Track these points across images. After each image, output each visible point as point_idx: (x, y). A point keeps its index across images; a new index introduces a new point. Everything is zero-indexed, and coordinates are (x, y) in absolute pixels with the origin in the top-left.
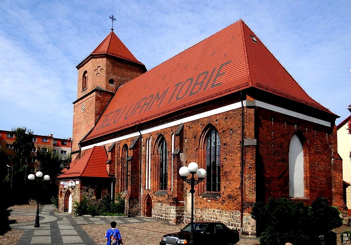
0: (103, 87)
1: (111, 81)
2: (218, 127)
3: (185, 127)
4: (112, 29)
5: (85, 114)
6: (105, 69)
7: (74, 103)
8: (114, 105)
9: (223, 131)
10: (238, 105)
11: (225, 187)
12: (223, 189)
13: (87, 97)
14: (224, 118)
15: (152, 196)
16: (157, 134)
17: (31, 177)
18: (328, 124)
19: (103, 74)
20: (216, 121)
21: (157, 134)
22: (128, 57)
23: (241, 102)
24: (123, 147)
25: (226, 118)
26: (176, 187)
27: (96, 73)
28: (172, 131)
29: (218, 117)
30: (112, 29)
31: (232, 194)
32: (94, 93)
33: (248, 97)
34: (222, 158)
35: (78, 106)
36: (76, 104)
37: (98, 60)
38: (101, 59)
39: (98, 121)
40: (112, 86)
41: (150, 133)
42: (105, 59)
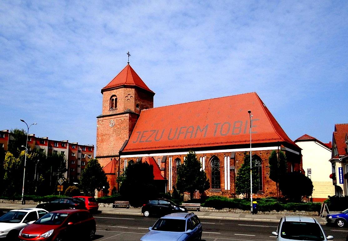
0: (133, 110)
1: (137, 106)
2: (262, 157)
3: (236, 154)
4: (128, 63)
5: (115, 128)
6: (134, 97)
7: (97, 117)
8: (140, 123)
9: (265, 160)
10: (276, 148)
11: (267, 188)
12: (266, 189)
13: (117, 116)
14: (266, 153)
15: (208, 193)
16: (211, 155)
17: (71, 192)
18: (298, 153)
19: (133, 100)
20: (261, 154)
21: (211, 155)
22: (142, 85)
23: (278, 147)
24: (175, 160)
25: (267, 153)
26: (234, 188)
27: (127, 99)
28: (225, 155)
29: (262, 152)
30: (128, 63)
31: (272, 192)
32: (128, 115)
33: (282, 146)
34: (265, 173)
35: (104, 120)
36: (100, 119)
37: (128, 89)
38: (131, 89)
39: (130, 135)
40: (138, 109)
41: (204, 154)
42: (133, 90)
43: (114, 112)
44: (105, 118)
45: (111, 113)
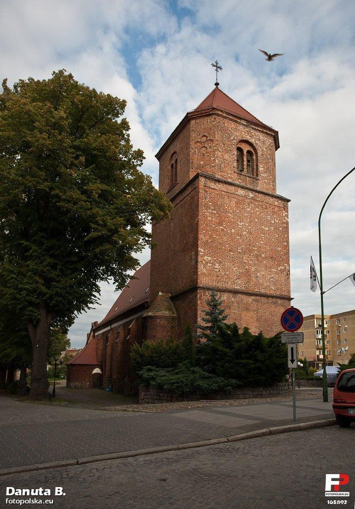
4: (217, 84)
30: (217, 84)
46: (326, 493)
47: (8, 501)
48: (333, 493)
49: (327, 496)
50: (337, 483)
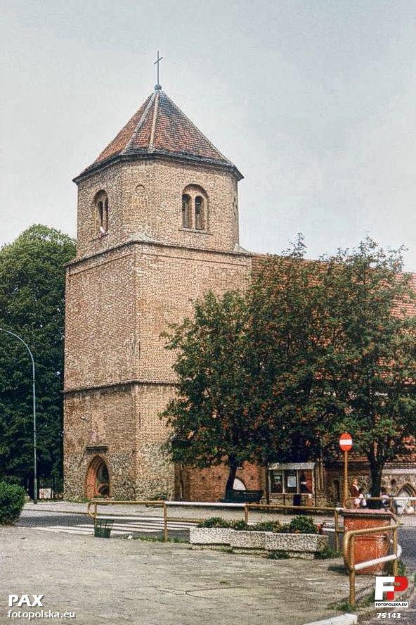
43: (201, 242)
44: (166, 252)
45: (187, 240)
46: (376, 602)
47: (11, 614)
48: (386, 603)
49: (377, 607)
50: (391, 589)
